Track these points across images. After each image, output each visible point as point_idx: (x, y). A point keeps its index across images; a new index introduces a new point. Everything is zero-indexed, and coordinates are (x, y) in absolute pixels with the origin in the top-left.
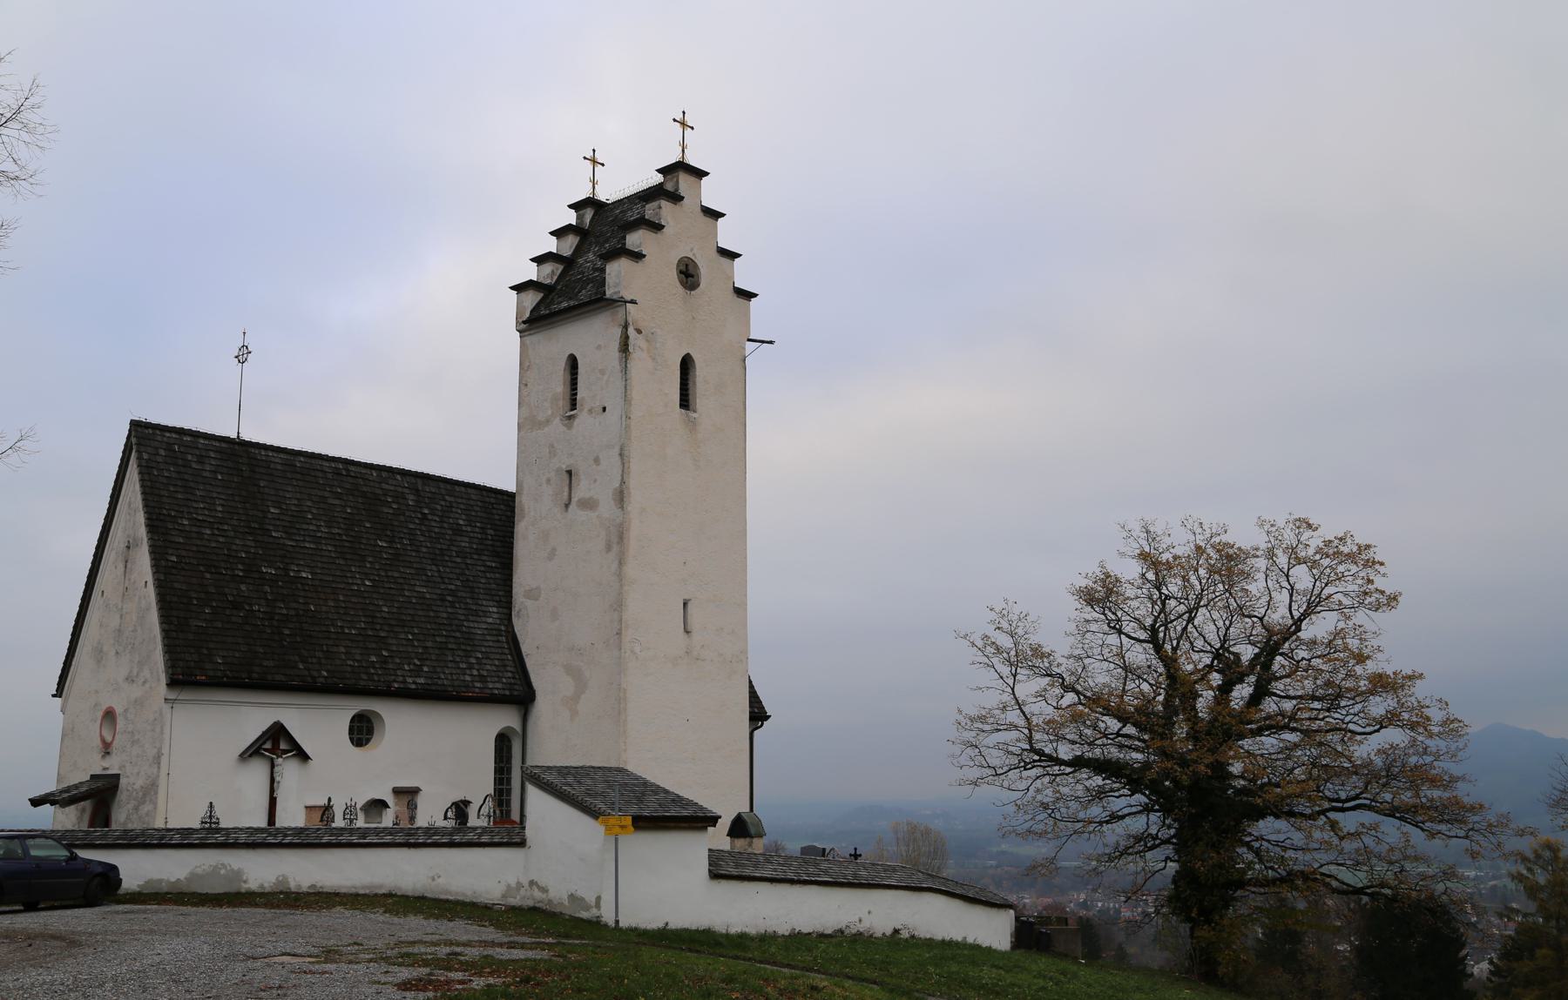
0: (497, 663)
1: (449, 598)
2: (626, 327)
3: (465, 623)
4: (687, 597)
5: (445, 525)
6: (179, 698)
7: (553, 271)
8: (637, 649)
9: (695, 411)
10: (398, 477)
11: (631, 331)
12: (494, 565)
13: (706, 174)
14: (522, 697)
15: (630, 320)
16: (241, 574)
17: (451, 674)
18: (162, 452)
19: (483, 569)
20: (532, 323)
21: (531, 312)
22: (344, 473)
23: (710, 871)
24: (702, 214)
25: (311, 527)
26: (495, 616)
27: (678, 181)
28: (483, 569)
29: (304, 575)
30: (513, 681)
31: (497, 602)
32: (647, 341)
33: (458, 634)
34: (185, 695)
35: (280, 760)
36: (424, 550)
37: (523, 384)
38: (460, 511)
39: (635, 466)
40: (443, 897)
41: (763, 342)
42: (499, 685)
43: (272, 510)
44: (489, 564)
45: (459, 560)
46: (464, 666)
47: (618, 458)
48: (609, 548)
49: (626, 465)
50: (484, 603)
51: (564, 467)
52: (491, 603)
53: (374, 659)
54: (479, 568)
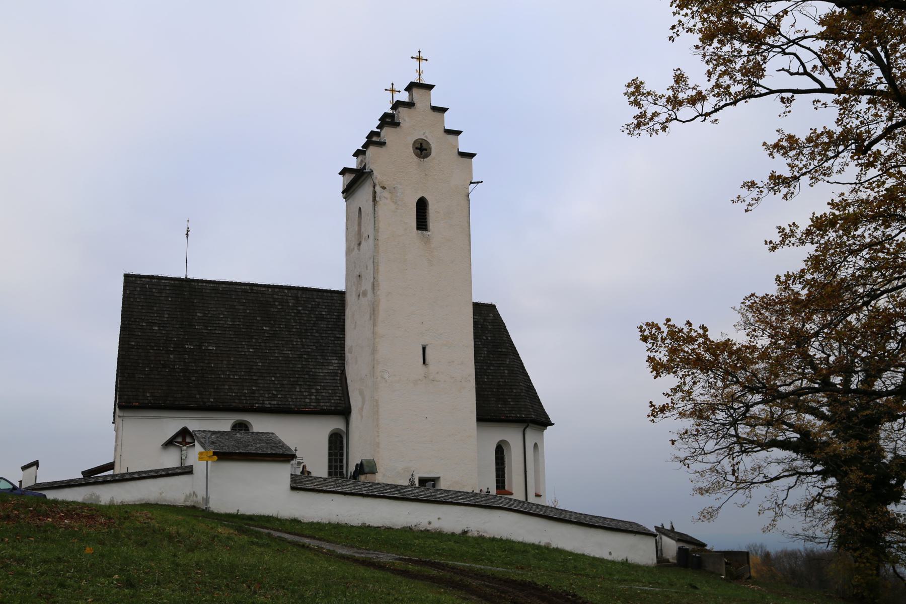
1: (305, 356)
2: (374, 187)
4: (424, 344)
8: (386, 376)
10: (286, 291)
11: (378, 189)
14: (344, 411)
15: (376, 182)
16: (172, 349)
18: (139, 289)
20: (348, 191)
22: (250, 291)
25: (221, 322)
29: (211, 348)
30: (338, 401)
35: (185, 448)
36: (294, 330)
37: (347, 229)
38: (324, 307)
39: (382, 268)
41: (478, 183)
42: (328, 404)
43: (199, 315)
44: (338, 336)
45: (317, 335)
46: (307, 394)
48: (371, 319)
51: (358, 273)
52: (335, 358)
54: (330, 338)
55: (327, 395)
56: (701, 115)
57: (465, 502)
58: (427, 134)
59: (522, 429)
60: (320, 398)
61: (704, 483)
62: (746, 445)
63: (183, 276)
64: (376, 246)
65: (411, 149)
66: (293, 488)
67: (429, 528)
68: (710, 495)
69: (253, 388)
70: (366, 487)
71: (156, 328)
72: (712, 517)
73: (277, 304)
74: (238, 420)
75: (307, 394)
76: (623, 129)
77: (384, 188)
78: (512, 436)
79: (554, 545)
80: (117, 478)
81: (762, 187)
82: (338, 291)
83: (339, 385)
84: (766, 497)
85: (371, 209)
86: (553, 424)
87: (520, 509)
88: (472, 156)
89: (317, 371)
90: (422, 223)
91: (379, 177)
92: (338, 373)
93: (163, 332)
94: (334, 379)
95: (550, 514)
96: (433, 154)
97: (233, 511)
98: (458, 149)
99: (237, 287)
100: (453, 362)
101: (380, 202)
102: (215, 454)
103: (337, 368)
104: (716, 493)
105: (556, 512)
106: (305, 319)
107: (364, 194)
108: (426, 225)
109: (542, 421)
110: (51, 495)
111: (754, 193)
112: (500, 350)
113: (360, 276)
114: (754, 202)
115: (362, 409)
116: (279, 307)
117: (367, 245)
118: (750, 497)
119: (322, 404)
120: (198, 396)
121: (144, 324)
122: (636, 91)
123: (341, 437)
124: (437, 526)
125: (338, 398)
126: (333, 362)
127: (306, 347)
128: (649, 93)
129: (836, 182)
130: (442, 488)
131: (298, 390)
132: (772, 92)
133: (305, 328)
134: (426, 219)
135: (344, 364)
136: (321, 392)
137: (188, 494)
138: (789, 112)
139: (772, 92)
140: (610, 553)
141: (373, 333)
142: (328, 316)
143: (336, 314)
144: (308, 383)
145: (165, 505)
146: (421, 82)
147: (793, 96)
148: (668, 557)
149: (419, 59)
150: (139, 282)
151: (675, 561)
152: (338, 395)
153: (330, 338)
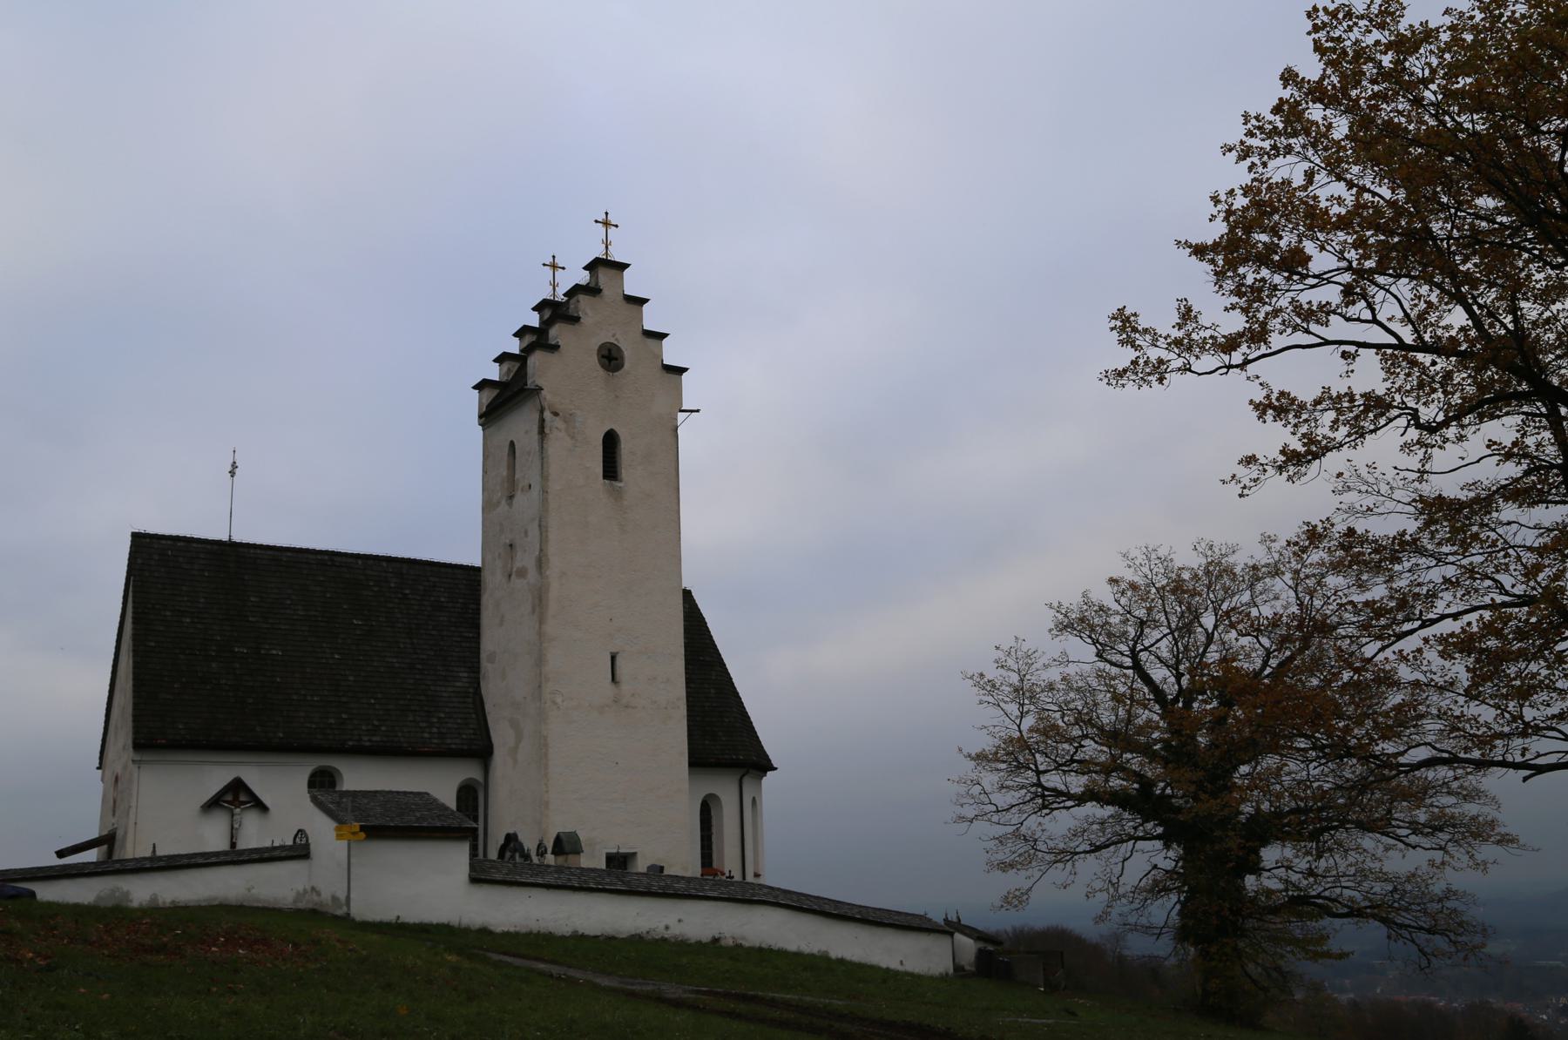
0: (459, 721)
1: (419, 666)
2: (542, 411)
3: (432, 688)
4: (614, 650)
5: (426, 603)
6: (144, 759)
7: (509, 369)
8: (559, 700)
9: (621, 481)
10: (384, 564)
11: (547, 415)
12: (471, 635)
13: (627, 266)
14: (481, 751)
15: (545, 404)
16: (213, 654)
17: (409, 732)
18: (156, 557)
19: (459, 639)
20: (489, 416)
21: (487, 407)
22: (329, 563)
23: (470, 875)
24: (624, 302)
25: (288, 611)
26: (465, 680)
27: (597, 277)
28: (459, 639)
29: (274, 652)
30: (473, 737)
31: (469, 668)
32: (565, 422)
33: (422, 698)
34: (146, 757)
35: (238, 810)
36: (400, 625)
37: (485, 472)
38: (442, 590)
39: (553, 535)
40: (255, 905)
41: (692, 411)
42: (458, 741)
43: (252, 599)
44: (467, 635)
45: (434, 632)
46: (424, 725)
47: (537, 528)
48: (533, 612)
49: (544, 534)
50: (456, 669)
51: (508, 541)
52: (463, 669)
53: (332, 721)
54: (454, 639)
55: (456, 726)
56: (1225, 367)
57: (715, 894)
58: (617, 336)
59: (739, 777)
60: (444, 731)
61: (1004, 855)
62: (1047, 799)
63: (225, 538)
64: (544, 501)
65: (595, 358)
66: (475, 880)
67: (666, 936)
68: (1019, 872)
69: (344, 716)
70: (575, 875)
71: (188, 620)
72: (1020, 902)
73: (371, 584)
74: (320, 766)
75: (424, 725)
76: (1100, 376)
77: (556, 414)
78: (724, 789)
79: (834, 955)
80: (162, 864)
81: (1266, 464)
82: (462, 565)
83: (471, 711)
84: (1095, 874)
85: (535, 445)
86: (776, 769)
87: (789, 903)
88: (681, 370)
89: (438, 688)
90: (611, 470)
91: (549, 397)
92: (469, 693)
93: (199, 626)
94: (464, 702)
95: (827, 908)
96: (627, 365)
97: (389, 916)
98: (662, 361)
99: (311, 556)
100: (655, 678)
101: (551, 436)
102: (362, 828)
103: (467, 685)
104: (1027, 870)
105: (795, 898)
106: (416, 607)
107: (521, 425)
108: (615, 472)
109: (760, 764)
110: (47, 892)
111: (1254, 471)
112: (701, 658)
113: (511, 545)
114: (1252, 484)
115: (514, 751)
116: (376, 589)
117: (526, 503)
118: (1075, 874)
119: (449, 741)
120: (258, 729)
121: (168, 613)
122: (1126, 325)
123: (476, 791)
124: (677, 932)
125: (471, 731)
126: (461, 675)
127: (419, 651)
128: (1146, 331)
129: (1407, 470)
130: (582, 866)
131: (411, 718)
132: (1327, 343)
133: (415, 621)
134: (615, 462)
135: (479, 678)
136: (447, 723)
137: (301, 888)
138: (1352, 371)
139: (1327, 343)
140: (901, 963)
141: (540, 634)
142: (450, 605)
143: (460, 601)
144: (426, 708)
145: (258, 908)
146: (609, 258)
147: (1357, 351)
148: (963, 963)
149: (606, 224)
150: (156, 546)
151: (973, 969)
152: (471, 726)
153: (454, 639)
